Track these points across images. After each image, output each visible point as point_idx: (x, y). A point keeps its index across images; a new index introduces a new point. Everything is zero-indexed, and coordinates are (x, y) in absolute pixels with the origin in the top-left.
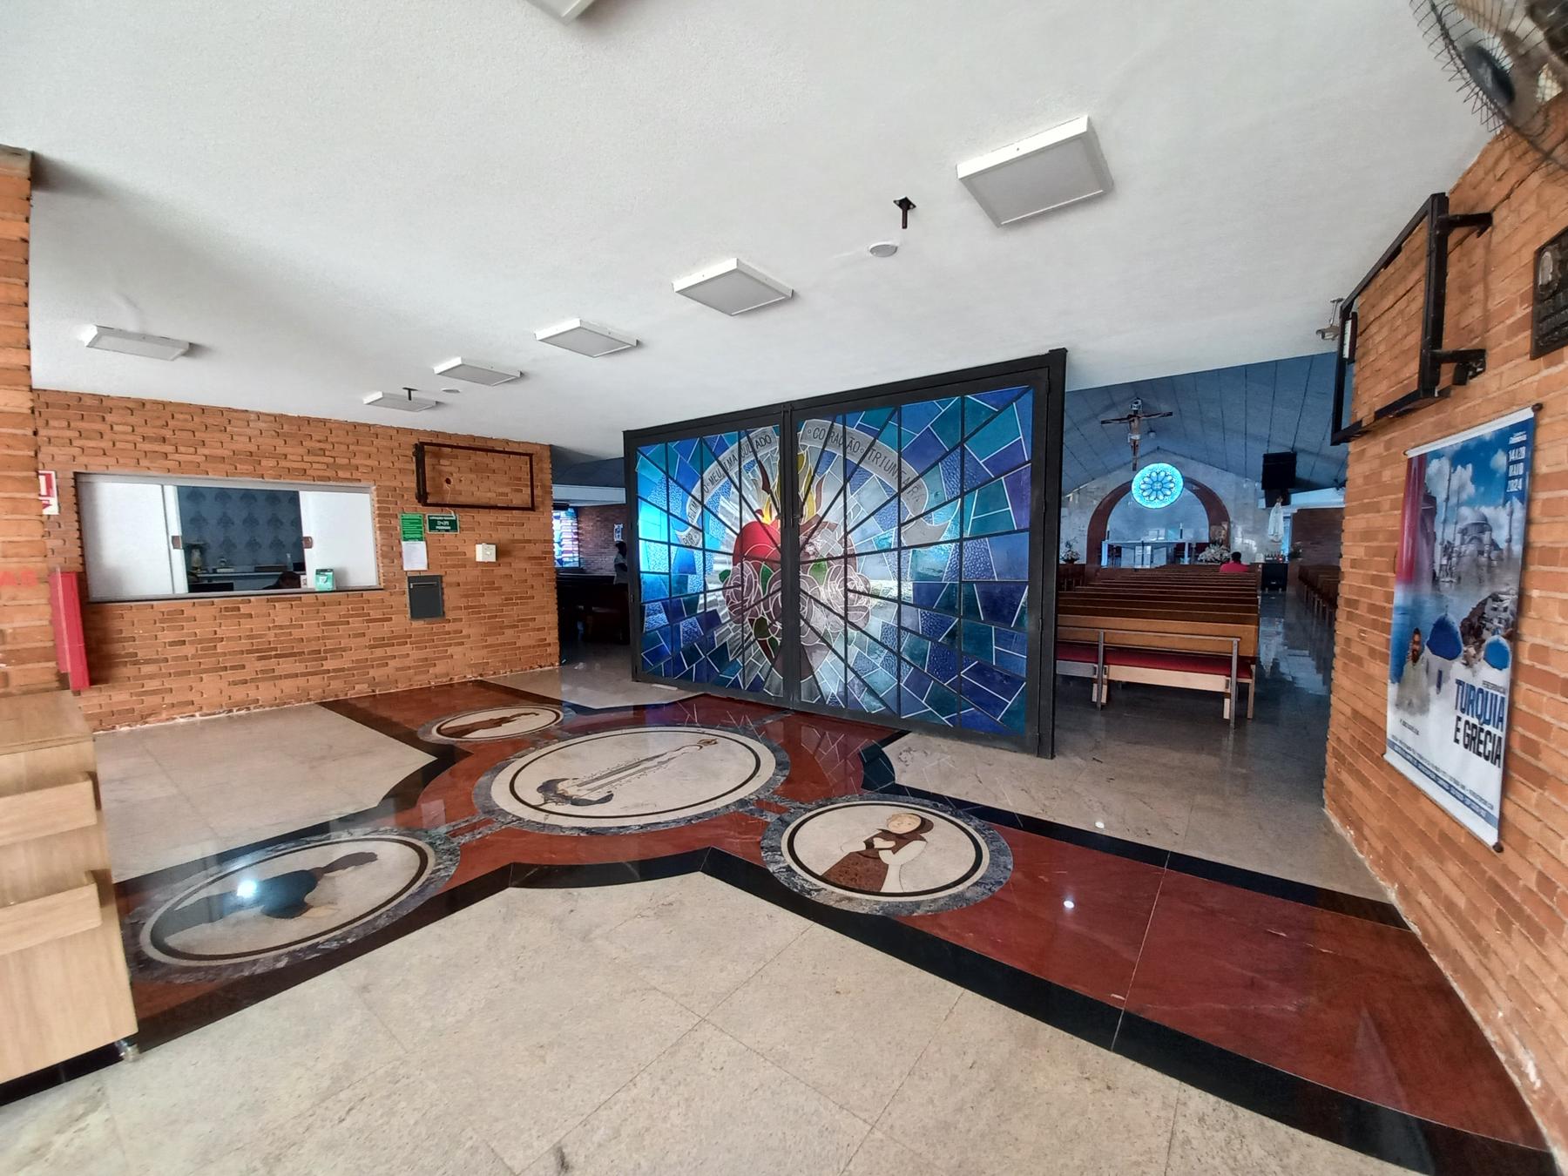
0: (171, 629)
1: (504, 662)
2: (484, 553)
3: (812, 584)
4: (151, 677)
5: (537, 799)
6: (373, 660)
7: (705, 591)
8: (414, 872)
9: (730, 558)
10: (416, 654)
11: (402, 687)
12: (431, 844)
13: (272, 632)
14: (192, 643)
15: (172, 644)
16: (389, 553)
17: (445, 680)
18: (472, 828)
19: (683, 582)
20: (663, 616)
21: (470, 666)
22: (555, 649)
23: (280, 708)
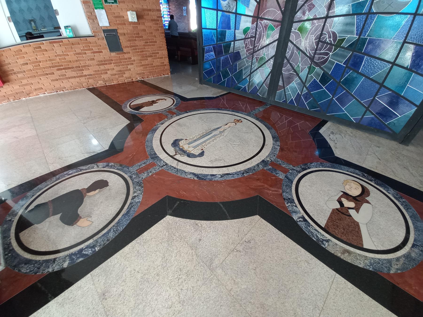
0: (21, 58)
1: (150, 72)
2: (131, 17)
3: (298, 37)
4: (23, 78)
5: (171, 150)
6: (101, 71)
7: (235, 40)
8: (124, 196)
9: (251, 19)
10: (117, 69)
11: (115, 83)
12: (131, 177)
13: (58, 58)
14: (30, 64)
15: (24, 64)
16: (92, 18)
17: (130, 80)
18: (146, 169)
19: (223, 35)
20: (213, 53)
21: (138, 74)
22: (168, 67)
23: (74, 90)
